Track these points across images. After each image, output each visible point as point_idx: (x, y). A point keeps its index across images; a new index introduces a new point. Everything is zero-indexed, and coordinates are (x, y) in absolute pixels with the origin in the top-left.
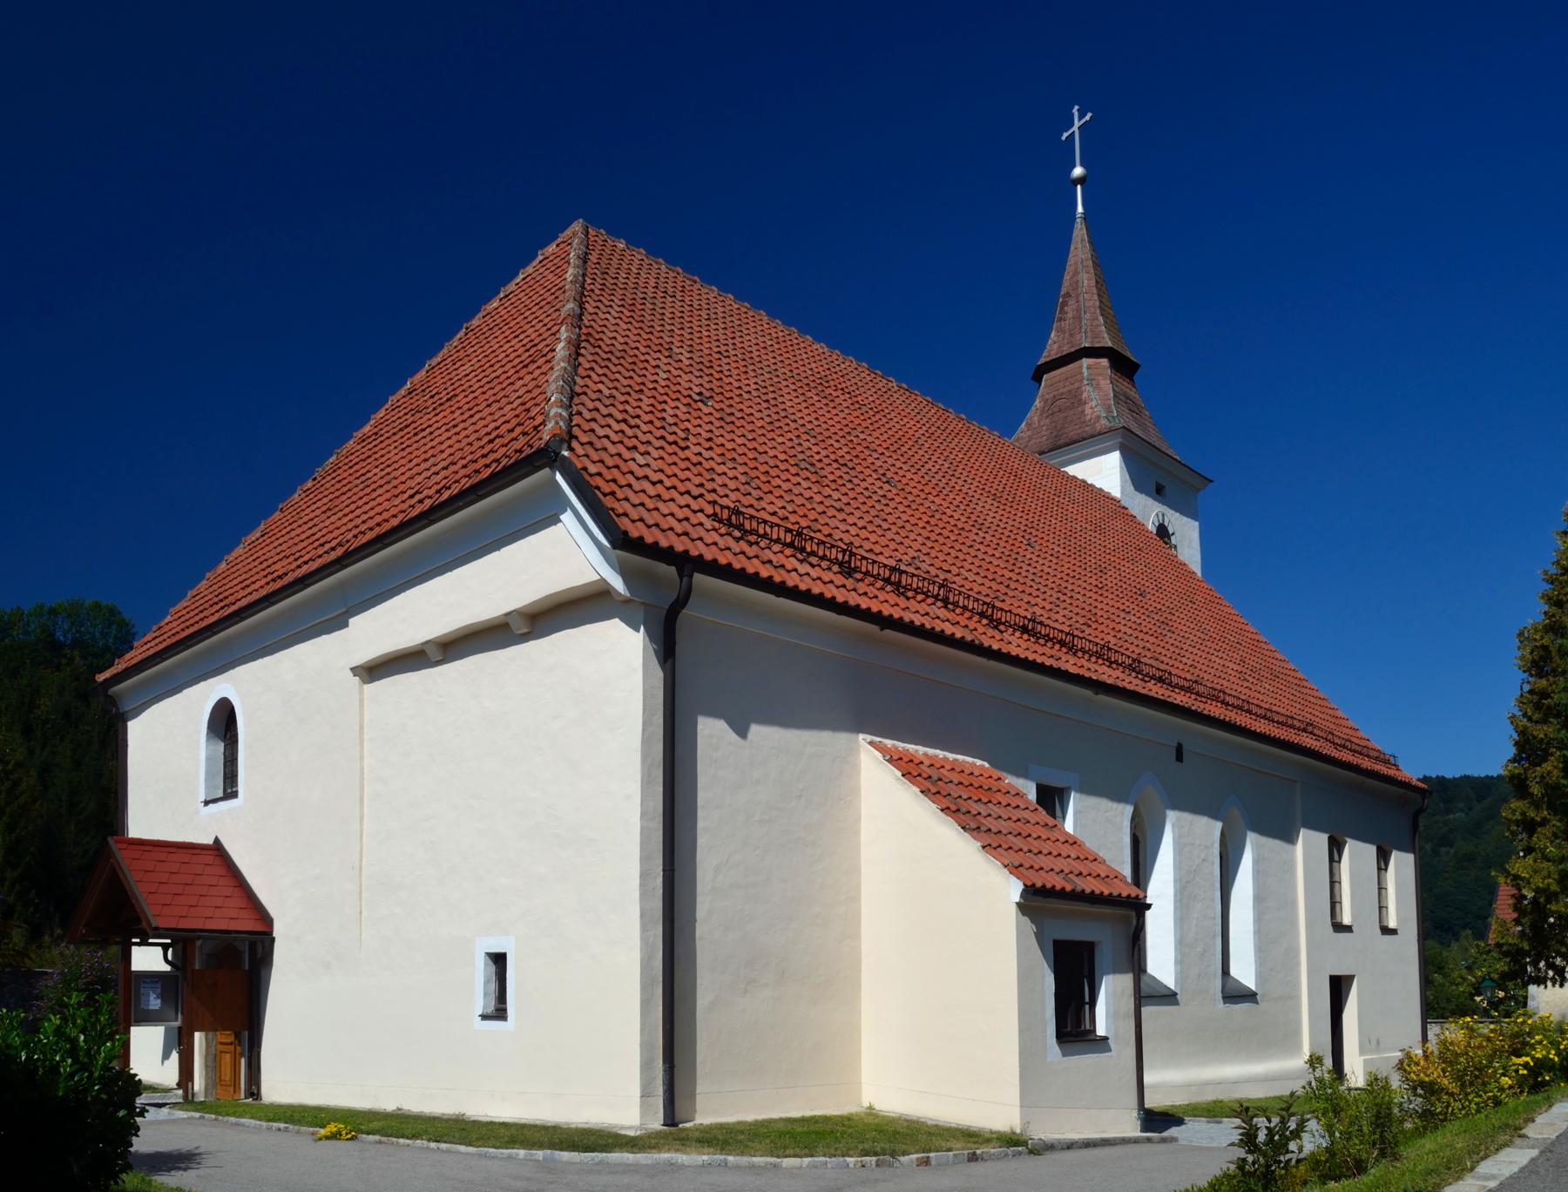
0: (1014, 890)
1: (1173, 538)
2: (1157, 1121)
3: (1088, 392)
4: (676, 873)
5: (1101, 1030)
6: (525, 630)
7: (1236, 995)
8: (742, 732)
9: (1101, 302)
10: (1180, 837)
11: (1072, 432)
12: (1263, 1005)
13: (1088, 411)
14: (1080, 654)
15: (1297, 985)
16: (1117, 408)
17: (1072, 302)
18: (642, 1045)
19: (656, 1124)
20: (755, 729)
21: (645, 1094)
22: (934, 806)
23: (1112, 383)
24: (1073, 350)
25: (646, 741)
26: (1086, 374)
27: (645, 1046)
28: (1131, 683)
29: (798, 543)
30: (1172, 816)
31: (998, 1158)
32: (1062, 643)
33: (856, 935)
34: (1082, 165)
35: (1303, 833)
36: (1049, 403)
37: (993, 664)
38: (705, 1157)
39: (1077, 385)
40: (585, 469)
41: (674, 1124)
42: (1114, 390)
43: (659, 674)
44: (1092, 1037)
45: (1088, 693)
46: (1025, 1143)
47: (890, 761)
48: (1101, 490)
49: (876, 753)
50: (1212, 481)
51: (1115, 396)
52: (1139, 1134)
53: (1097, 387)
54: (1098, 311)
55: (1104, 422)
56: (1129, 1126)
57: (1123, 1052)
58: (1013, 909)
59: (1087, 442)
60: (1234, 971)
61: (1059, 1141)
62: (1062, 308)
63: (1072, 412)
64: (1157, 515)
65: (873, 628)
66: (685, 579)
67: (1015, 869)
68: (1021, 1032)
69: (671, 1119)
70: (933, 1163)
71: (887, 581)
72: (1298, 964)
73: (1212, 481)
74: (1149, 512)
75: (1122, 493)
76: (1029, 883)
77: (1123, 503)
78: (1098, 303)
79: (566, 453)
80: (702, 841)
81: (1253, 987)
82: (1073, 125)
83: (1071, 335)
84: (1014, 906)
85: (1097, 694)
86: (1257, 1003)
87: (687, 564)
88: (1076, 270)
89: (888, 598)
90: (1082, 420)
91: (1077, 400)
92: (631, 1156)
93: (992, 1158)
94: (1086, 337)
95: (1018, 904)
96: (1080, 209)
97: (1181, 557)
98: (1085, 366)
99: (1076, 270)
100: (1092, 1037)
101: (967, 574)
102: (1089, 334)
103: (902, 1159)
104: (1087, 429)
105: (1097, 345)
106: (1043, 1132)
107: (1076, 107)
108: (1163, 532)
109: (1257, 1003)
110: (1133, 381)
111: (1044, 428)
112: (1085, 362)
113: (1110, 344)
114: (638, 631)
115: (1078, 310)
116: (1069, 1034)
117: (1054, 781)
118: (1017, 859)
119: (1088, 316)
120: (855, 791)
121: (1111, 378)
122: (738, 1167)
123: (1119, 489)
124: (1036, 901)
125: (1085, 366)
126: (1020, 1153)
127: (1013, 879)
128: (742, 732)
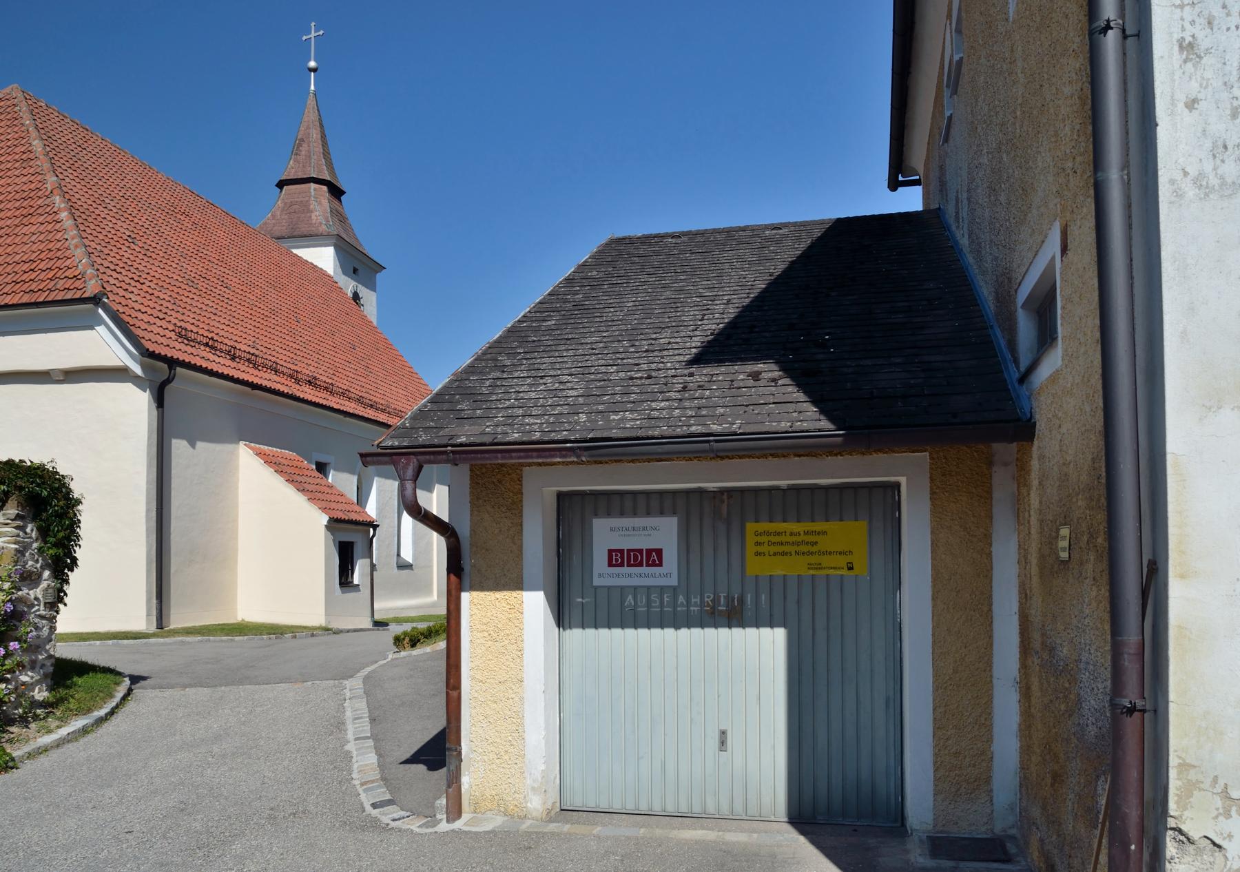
0: (324, 519)
1: (361, 300)
2: (379, 624)
3: (313, 205)
4: (164, 510)
5: (356, 581)
6: (61, 379)
7: (404, 566)
8: (193, 445)
9: (324, 150)
10: (380, 486)
11: (304, 229)
12: (416, 571)
13: (313, 217)
14: (335, 395)
15: (431, 560)
16: (332, 218)
17: (305, 145)
18: (147, 592)
19: (153, 628)
20: (200, 445)
21: (148, 615)
22: (282, 479)
23: (329, 202)
24: (305, 177)
25: (149, 446)
26: (313, 194)
27: (148, 592)
28: (360, 411)
29: (211, 345)
30: (376, 479)
31: (322, 635)
32: (327, 389)
33: (236, 538)
34: (315, 60)
35: (437, 486)
36: (288, 206)
37: (300, 404)
38: (199, 638)
39: (307, 199)
40: (118, 311)
41: (162, 628)
42: (330, 207)
43: (155, 413)
44: (351, 585)
45: (341, 417)
46: (331, 630)
47: (256, 454)
48: (321, 269)
49: (250, 450)
50: (385, 268)
51: (331, 211)
52: (371, 627)
53: (320, 204)
54: (322, 156)
55: (324, 227)
56: (367, 624)
57: (365, 591)
58: (323, 528)
59: (312, 238)
60: (403, 555)
61: (344, 629)
62: (298, 147)
63: (303, 215)
64: (353, 286)
65: (249, 389)
66: (173, 371)
67: (324, 510)
68: (326, 582)
69: (160, 625)
70: (298, 637)
71: (248, 360)
72: (433, 550)
73: (385, 268)
74: (349, 286)
75: (334, 272)
76: (331, 517)
77: (336, 279)
78: (322, 150)
79: (106, 300)
80: (173, 493)
81: (411, 562)
82: (311, 34)
83: (304, 167)
84: (324, 527)
85: (345, 417)
86: (413, 570)
87: (172, 363)
88: (309, 125)
89: (103, 263)
90: (310, 222)
91: (306, 209)
92: (162, 640)
93: (319, 635)
94: (314, 171)
95: (326, 526)
96: (312, 88)
97: (365, 313)
98: (312, 188)
99: (309, 125)
100: (351, 585)
101: (152, 243)
102: (316, 168)
103: (286, 635)
104: (313, 229)
105: (320, 177)
106: (335, 625)
107: (313, 24)
108: (356, 297)
109: (413, 570)
110: (341, 201)
111: (284, 221)
112: (313, 186)
113: (329, 179)
114: (145, 392)
115: (309, 151)
116: (343, 583)
117: (322, 459)
118: (324, 504)
119: (315, 157)
120: (237, 468)
121: (329, 199)
122: (215, 641)
123: (332, 270)
124: (335, 524)
125: (312, 188)
126: (330, 634)
127: (324, 515)
128: (193, 445)
